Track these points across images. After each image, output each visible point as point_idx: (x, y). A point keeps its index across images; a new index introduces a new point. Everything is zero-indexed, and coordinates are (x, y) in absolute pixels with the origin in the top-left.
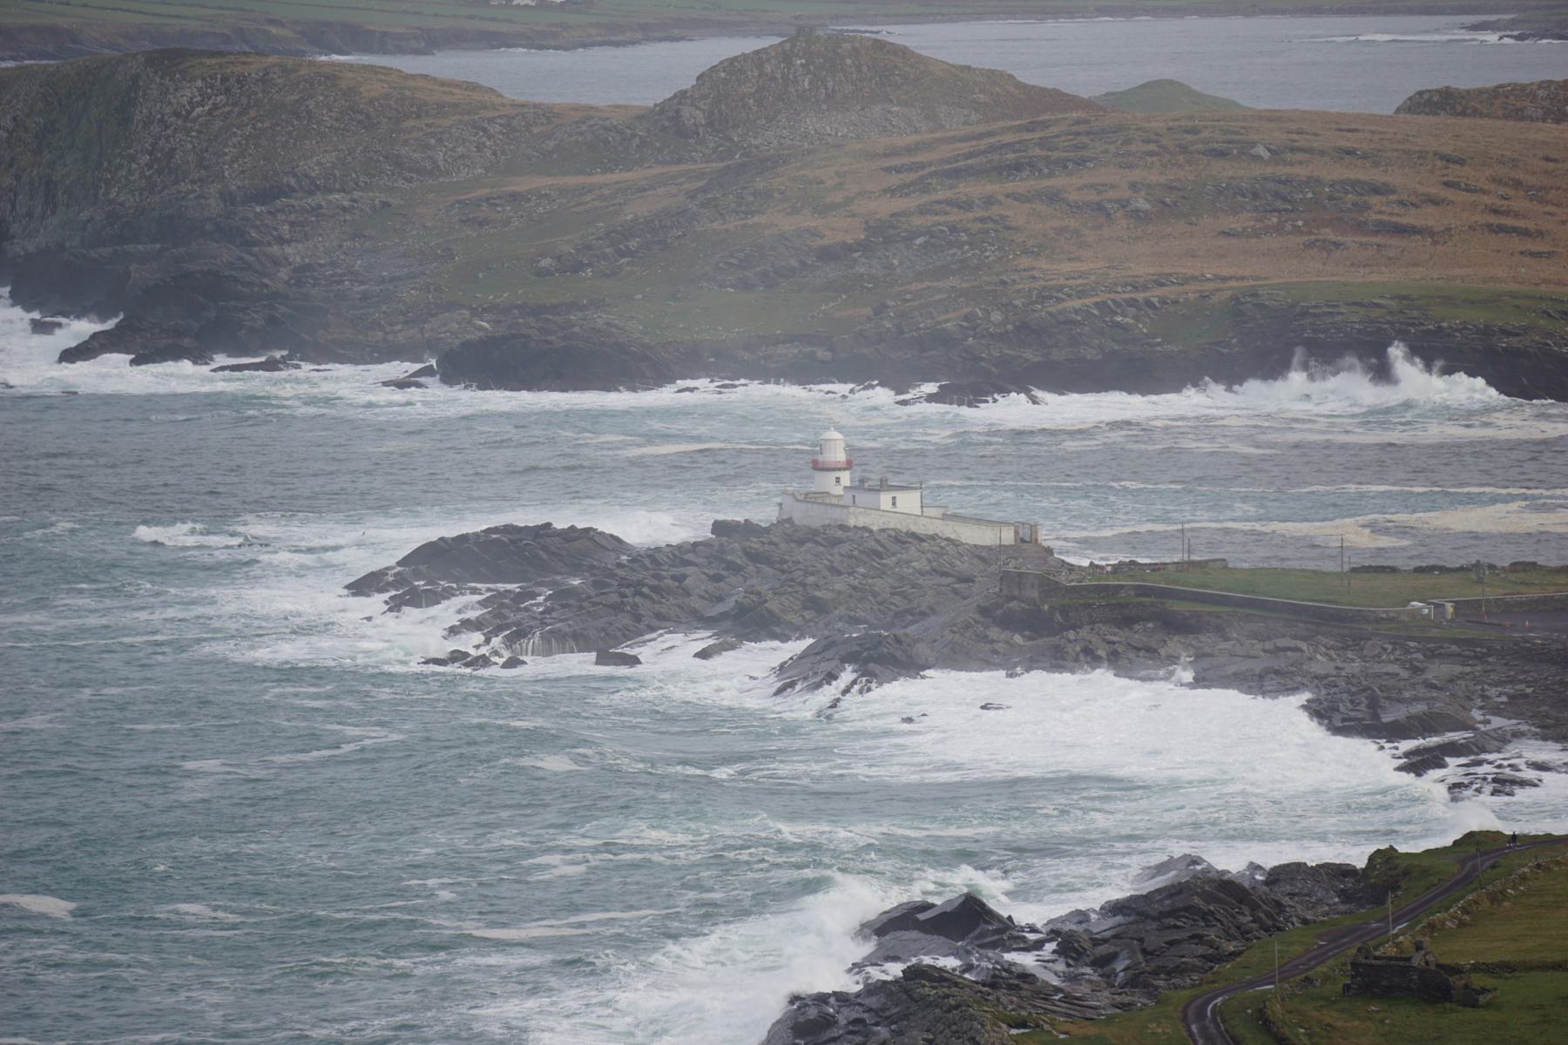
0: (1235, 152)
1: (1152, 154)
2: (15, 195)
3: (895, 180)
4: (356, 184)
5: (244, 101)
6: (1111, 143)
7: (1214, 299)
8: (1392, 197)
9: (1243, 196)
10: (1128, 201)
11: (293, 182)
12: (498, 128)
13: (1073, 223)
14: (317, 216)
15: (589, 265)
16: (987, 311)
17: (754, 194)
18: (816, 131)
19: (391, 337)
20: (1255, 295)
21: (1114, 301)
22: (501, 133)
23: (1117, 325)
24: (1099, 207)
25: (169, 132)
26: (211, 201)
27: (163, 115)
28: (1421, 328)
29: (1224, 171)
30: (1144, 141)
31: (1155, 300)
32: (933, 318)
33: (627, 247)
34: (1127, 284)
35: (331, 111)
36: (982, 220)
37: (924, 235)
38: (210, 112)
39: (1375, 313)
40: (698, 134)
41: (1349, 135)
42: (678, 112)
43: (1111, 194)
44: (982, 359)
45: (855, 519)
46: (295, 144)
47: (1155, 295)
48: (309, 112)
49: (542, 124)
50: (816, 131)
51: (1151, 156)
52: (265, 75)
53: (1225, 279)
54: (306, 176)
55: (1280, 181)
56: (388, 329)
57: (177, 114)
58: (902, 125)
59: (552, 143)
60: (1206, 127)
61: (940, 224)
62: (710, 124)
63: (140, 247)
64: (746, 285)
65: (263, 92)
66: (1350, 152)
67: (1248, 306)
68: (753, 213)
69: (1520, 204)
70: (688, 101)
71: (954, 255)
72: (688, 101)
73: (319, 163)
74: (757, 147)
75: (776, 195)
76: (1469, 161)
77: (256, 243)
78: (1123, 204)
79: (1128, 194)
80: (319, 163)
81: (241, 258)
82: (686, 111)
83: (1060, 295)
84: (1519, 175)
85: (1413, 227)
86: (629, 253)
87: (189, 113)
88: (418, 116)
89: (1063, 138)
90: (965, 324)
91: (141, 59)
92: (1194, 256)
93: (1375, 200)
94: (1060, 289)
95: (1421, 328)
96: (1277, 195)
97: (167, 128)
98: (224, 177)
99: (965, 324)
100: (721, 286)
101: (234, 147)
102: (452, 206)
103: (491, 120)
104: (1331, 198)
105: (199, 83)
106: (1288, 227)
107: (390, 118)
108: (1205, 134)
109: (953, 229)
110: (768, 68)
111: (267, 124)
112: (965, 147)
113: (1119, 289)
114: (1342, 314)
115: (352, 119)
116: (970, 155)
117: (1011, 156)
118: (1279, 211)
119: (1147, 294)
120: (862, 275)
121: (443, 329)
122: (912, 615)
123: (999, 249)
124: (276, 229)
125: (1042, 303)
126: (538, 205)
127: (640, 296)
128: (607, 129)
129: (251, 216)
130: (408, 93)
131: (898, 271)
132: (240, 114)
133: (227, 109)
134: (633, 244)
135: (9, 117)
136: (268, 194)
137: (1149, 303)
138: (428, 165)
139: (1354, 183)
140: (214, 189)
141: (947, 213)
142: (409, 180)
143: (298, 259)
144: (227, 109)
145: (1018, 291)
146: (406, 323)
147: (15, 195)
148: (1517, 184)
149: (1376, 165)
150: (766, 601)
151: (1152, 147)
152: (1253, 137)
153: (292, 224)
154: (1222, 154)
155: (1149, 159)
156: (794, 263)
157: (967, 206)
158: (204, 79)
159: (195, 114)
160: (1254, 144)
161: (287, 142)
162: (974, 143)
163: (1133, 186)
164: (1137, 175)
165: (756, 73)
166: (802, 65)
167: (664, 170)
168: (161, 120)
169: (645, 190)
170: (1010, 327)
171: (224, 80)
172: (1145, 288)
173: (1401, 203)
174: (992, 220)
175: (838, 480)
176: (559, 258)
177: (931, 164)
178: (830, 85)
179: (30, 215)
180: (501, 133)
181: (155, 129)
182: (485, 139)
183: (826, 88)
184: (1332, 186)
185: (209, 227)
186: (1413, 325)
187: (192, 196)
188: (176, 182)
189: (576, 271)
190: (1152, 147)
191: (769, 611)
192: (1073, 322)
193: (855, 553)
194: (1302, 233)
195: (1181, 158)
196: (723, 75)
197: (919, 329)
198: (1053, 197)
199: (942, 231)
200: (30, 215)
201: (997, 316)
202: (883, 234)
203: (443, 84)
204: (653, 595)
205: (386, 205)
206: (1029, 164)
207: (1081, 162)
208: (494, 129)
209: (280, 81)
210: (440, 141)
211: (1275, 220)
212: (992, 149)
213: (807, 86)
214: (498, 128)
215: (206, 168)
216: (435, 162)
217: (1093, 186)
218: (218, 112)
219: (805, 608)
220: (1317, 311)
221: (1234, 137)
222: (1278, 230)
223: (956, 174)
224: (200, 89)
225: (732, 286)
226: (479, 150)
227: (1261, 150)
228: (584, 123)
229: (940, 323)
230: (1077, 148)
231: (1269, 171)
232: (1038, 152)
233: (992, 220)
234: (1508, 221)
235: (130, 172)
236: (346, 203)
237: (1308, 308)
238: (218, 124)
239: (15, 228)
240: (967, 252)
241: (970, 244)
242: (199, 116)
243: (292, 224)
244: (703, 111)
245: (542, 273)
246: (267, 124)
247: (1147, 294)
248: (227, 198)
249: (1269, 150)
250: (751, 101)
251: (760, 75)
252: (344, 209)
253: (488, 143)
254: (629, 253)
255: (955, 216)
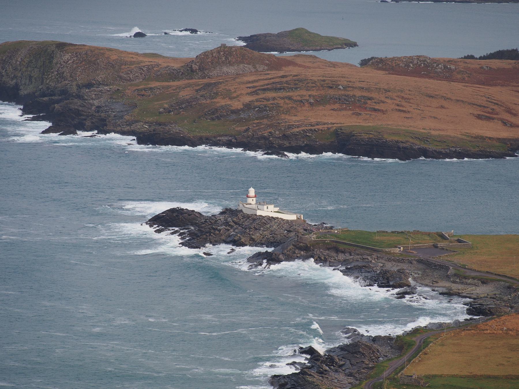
0: (334, 87)
1: (314, 87)
2: (21, 78)
3: (249, 90)
4: (110, 83)
5: (81, 59)
6: (303, 84)
7: (331, 130)
8: (373, 101)
9: (337, 99)
10: (308, 100)
11: (94, 82)
12: (146, 69)
13: (294, 106)
14: (101, 93)
15: (173, 111)
16: (275, 131)
17: (214, 93)
18: (226, 71)
19: (123, 129)
20: (341, 129)
21: (306, 129)
22: (146, 70)
23: (308, 136)
24: (301, 101)
25: (62, 66)
26: (74, 87)
27: (61, 62)
28: (382, 141)
29: (331, 92)
30: (312, 83)
31: (316, 129)
32: (261, 132)
33: (182, 107)
34: (309, 125)
35: (103, 63)
36: (272, 104)
37: (257, 107)
38: (73, 62)
39: (371, 136)
40: (196, 71)
41: (362, 83)
42: (191, 66)
43: (305, 98)
44: (274, 144)
45: (259, 213)
46: (94, 72)
47: (316, 127)
48: (98, 63)
49: (157, 67)
50: (226, 71)
51: (314, 87)
52: (86, 53)
53: (334, 124)
54: (98, 81)
55: (346, 96)
56: (122, 127)
57: (64, 62)
58: (248, 70)
59: (159, 73)
60: (327, 80)
61: (262, 105)
62: (200, 69)
63: (56, 97)
64: (213, 119)
65: (86, 57)
66: (363, 88)
67: (340, 132)
68: (213, 98)
69: (404, 103)
70: (194, 63)
71: (265, 113)
72: (194, 63)
73: (101, 77)
74: (211, 76)
75: (219, 94)
76: (391, 91)
77: (87, 100)
78: (307, 101)
79: (308, 98)
80: (101, 77)
81: (82, 104)
82: (194, 66)
83: (293, 127)
84: (403, 95)
85: (378, 109)
86: (182, 108)
87: (68, 62)
88: (125, 65)
89: (291, 81)
90: (270, 134)
91: (54, 46)
92: (325, 116)
93: (369, 102)
94: (293, 125)
95: (382, 141)
96: (345, 99)
97: (61, 65)
98: (77, 80)
99: (270, 134)
100: (206, 119)
101: (79, 72)
102: (135, 90)
103: (144, 66)
104: (358, 101)
105: (70, 54)
106: (348, 108)
107: (118, 65)
108: (327, 82)
109: (265, 106)
110: (214, 55)
111: (87, 66)
112: (266, 82)
113: (308, 126)
114: (363, 136)
115: (109, 65)
116: (268, 85)
117: (279, 86)
118: (345, 104)
119: (314, 128)
120: (242, 118)
121: (136, 128)
122: (276, 243)
123: (277, 112)
124: (91, 96)
125: (289, 129)
126: (157, 91)
127: (186, 121)
128: (174, 70)
129: (85, 92)
130: (122, 58)
131: (251, 117)
132: (81, 63)
133: (77, 61)
134: (183, 106)
135: (20, 58)
136: (89, 85)
137: (315, 130)
138: (128, 78)
139: (364, 97)
140: (75, 83)
141: (263, 102)
142: (124, 82)
143: (97, 104)
144: (77, 61)
145: (283, 126)
146: (126, 125)
147: (21, 78)
148: (403, 98)
149: (369, 92)
150: (241, 239)
151: (314, 85)
152: (339, 83)
153: (95, 95)
154: (331, 88)
155: (313, 88)
156: (225, 114)
157: (268, 100)
158: (71, 53)
159: (69, 62)
160: (339, 85)
161: (92, 71)
162: (269, 81)
163: (310, 96)
164: (310, 93)
165: (211, 56)
166: (223, 54)
167: (188, 82)
168: (60, 63)
169: (184, 88)
170: (281, 135)
171: (76, 54)
172: (314, 126)
173: (375, 102)
174: (275, 104)
175: (253, 200)
176: (164, 109)
177: (258, 86)
178: (230, 59)
179: (25, 84)
180: (146, 70)
181: (59, 65)
182: (142, 72)
183: (229, 60)
184: (358, 97)
185: (74, 94)
186: (380, 140)
187: (69, 85)
188: (64, 81)
189: (169, 112)
190: (314, 85)
191: (242, 241)
192: (297, 135)
193: (260, 223)
194: (351, 110)
195: (321, 88)
196: (203, 56)
197: (258, 135)
198: (290, 98)
199: (262, 107)
200: (25, 84)
201: (277, 132)
202: (248, 107)
203: (130, 54)
204: (213, 235)
205: (118, 89)
206: (283, 88)
207: (296, 88)
208: (145, 69)
209: (90, 54)
210: (131, 72)
211: (345, 106)
212: (273, 83)
213: (224, 60)
214: (146, 69)
215: (72, 77)
216: (130, 78)
217: (299, 96)
218: (75, 62)
219: (250, 240)
220: (357, 135)
221: (334, 83)
222: (345, 109)
223: (264, 90)
224: (70, 56)
225: (209, 119)
226: (141, 75)
227: (341, 87)
228: (167, 67)
229: (263, 134)
230: (295, 84)
231: (343, 92)
232: (285, 85)
233: (275, 104)
234: (401, 108)
235: (52, 76)
236: (109, 89)
237: (354, 134)
238: (75, 66)
239: (21, 87)
240: (269, 112)
241: (270, 110)
242: (70, 63)
243: (95, 95)
244: (198, 66)
245: (160, 113)
246: (87, 66)
247: (314, 128)
248: (78, 86)
249: (343, 87)
250: (210, 63)
251: (212, 56)
252: (108, 91)
253: (143, 73)
254: (182, 108)
255: (265, 103)
